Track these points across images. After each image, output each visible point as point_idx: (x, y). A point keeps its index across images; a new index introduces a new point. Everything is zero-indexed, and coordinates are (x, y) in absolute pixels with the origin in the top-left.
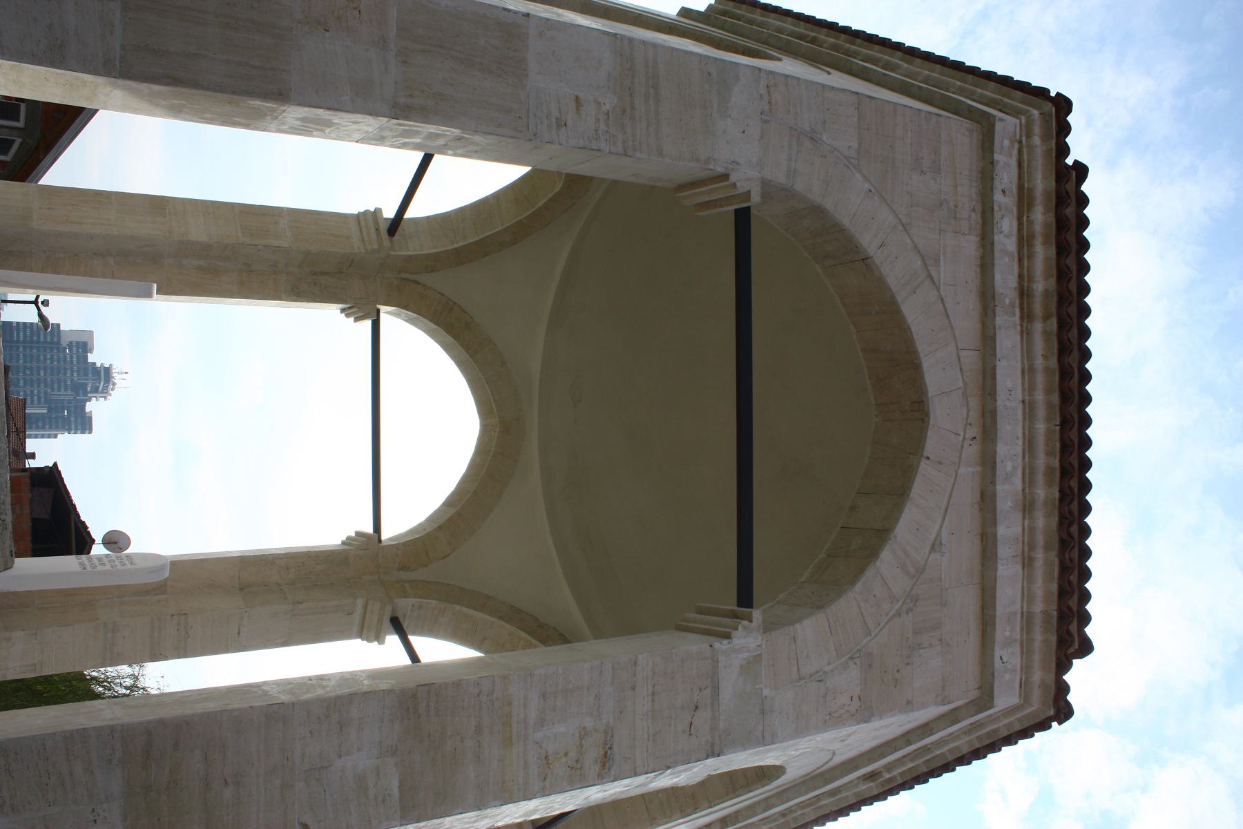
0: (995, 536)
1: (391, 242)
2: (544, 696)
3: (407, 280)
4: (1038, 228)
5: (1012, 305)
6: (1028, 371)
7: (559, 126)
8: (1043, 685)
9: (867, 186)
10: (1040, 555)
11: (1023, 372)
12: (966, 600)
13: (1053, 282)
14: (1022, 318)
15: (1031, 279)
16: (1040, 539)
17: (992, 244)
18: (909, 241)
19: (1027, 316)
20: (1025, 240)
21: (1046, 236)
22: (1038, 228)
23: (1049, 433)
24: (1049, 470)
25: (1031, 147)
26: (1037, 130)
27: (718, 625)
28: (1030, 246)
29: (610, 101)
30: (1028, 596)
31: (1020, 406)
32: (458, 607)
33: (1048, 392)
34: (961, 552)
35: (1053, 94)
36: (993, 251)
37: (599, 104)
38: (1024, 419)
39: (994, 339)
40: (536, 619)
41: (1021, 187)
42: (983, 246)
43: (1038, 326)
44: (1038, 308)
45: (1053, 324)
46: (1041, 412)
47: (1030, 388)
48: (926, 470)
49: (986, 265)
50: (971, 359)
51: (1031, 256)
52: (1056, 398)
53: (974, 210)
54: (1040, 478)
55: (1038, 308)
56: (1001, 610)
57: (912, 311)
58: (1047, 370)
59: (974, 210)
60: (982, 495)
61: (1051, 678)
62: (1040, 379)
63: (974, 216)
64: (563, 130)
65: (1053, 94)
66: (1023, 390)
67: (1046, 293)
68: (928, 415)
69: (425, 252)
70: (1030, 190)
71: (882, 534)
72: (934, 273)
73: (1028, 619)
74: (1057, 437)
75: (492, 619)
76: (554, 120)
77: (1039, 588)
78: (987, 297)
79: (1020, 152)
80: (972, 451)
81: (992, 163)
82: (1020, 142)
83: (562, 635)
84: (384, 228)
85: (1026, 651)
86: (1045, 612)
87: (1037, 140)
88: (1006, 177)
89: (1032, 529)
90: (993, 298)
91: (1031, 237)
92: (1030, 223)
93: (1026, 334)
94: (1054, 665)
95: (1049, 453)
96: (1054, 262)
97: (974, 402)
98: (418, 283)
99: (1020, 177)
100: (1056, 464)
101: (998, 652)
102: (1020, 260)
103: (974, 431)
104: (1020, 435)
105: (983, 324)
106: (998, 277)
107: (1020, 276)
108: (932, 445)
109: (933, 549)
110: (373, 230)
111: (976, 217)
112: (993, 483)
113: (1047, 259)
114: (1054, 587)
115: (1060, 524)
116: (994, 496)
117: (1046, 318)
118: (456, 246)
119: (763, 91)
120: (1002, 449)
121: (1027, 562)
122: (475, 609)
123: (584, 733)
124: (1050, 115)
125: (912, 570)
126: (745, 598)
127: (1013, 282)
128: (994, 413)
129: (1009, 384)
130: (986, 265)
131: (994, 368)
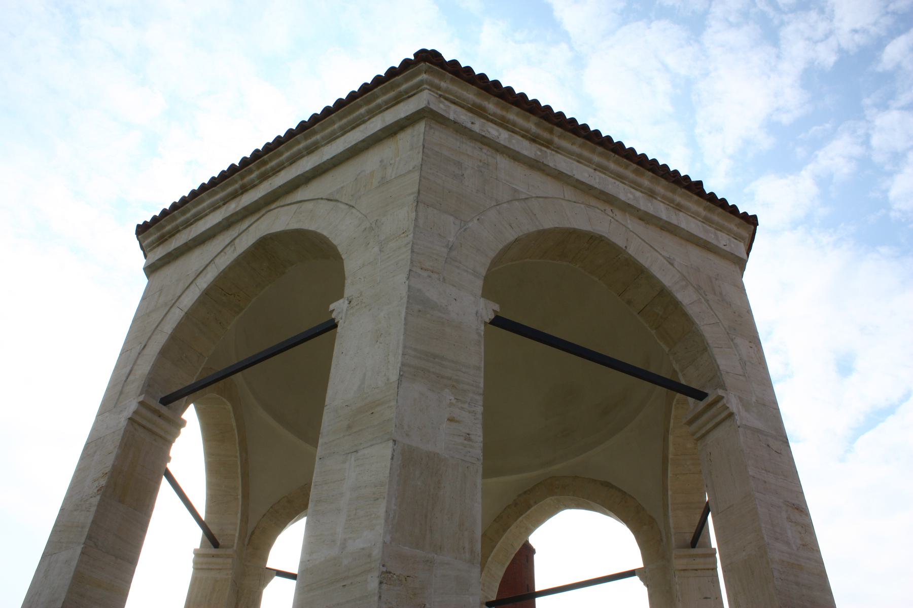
0: (666, 222)
1: (223, 547)
2: (777, 539)
3: (250, 539)
4: (499, 111)
5: (541, 151)
6: (580, 159)
7: (470, 440)
8: (738, 225)
9: (475, 221)
10: (678, 199)
11: (578, 162)
12: (696, 255)
13: (534, 119)
14: (548, 147)
15: (528, 131)
16: (669, 194)
17: (505, 147)
18: (505, 205)
19: (548, 144)
20: (503, 123)
21: (503, 108)
22: (499, 111)
23: (617, 162)
24: (635, 172)
25: (447, 91)
26: (437, 81)
27: (715, 416)
28: (508, 121)
29: (448, 396)
30: (695, 215)
31: (597, 173)
32: (490, 559)
33: (593, 151)
34: (670, 245)
35: (413, 58)
36: (509, 148)
37: (451, 405)
38: (605, 174)
39: (561, 173)
40: (509, 506)
41: (470, 110)
42: (502, 153)
43: (556, 140)
44: (546, 135)
45: (557, 130)
46: (604, 162)
47: (589, 162)
48: (631, 251)
49: (515, 157)
50: (569, 193)
51: (514, 124)
52: (600, 149)
53: (481, 149)
54: (639, 179)
55: (546, 135)
56: (701, 235)
57: (549, 222)
58: (581, 146)
59: (481, 149)
60: (641, 219)
61: (738, 220)
62: (586, 153)
63: (485, 151)
64: (473, 437)
65: (413, 58)
66: (588, 166)
67: (537, 125)
68: (601, 236)
69: (239, 522)
70: (474, 104)
71: (664, 294)
72: (524, 196)
73: (706, 221)
74: (621, 158)
75: (504, 537)
76: (466, 442)
77: (694, 207)
78: (535, 165)
79: (447, 99)
80: (619, 215)
81: (455, 123)
82: (440, 96)
83: (525, 493)
84: (213, 551)
85: (721, 228)
86: (705, 208)
87: (443, 85)
88: (464, 117)
89: (664, 197)
90: (537, 161)
91: (503, 118)
92: (494, 115)
93: (558, 150)
94: (732, 216)
95: (627, 167)
96: (523, 112)
97: (593, 202)
98: (253, 533)
99: (463, 107)
100: (635, 166)
101: (721, 246)
102: (513, 132)
103: (608, 208)
104: (613, 181)
105: (548, 175)
106: (525, 153)
107: (523, 136)
108: (619, 241)
109: (672, 264)
110: (214, 560)
111: (486, 149)
112: (638, 210)
113: (517, 114)
114: (696, 197)
115: (666, 179)
116: (646, 213)
117: (551, 132)
118: (240, 497)
119: (425, 274)
120: (622, 197)
121: (679, 208)
122: (494, 547)
123: (788, 518)
124: (430, 67)
125: (684, 283)
126: (700, 395)
127: (526, 143)
128: (602, 192)
129: (586, 175)
130: (515, 157)
131: (577, 180)
